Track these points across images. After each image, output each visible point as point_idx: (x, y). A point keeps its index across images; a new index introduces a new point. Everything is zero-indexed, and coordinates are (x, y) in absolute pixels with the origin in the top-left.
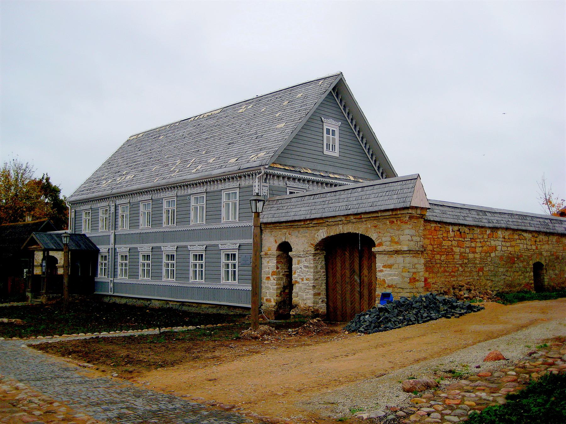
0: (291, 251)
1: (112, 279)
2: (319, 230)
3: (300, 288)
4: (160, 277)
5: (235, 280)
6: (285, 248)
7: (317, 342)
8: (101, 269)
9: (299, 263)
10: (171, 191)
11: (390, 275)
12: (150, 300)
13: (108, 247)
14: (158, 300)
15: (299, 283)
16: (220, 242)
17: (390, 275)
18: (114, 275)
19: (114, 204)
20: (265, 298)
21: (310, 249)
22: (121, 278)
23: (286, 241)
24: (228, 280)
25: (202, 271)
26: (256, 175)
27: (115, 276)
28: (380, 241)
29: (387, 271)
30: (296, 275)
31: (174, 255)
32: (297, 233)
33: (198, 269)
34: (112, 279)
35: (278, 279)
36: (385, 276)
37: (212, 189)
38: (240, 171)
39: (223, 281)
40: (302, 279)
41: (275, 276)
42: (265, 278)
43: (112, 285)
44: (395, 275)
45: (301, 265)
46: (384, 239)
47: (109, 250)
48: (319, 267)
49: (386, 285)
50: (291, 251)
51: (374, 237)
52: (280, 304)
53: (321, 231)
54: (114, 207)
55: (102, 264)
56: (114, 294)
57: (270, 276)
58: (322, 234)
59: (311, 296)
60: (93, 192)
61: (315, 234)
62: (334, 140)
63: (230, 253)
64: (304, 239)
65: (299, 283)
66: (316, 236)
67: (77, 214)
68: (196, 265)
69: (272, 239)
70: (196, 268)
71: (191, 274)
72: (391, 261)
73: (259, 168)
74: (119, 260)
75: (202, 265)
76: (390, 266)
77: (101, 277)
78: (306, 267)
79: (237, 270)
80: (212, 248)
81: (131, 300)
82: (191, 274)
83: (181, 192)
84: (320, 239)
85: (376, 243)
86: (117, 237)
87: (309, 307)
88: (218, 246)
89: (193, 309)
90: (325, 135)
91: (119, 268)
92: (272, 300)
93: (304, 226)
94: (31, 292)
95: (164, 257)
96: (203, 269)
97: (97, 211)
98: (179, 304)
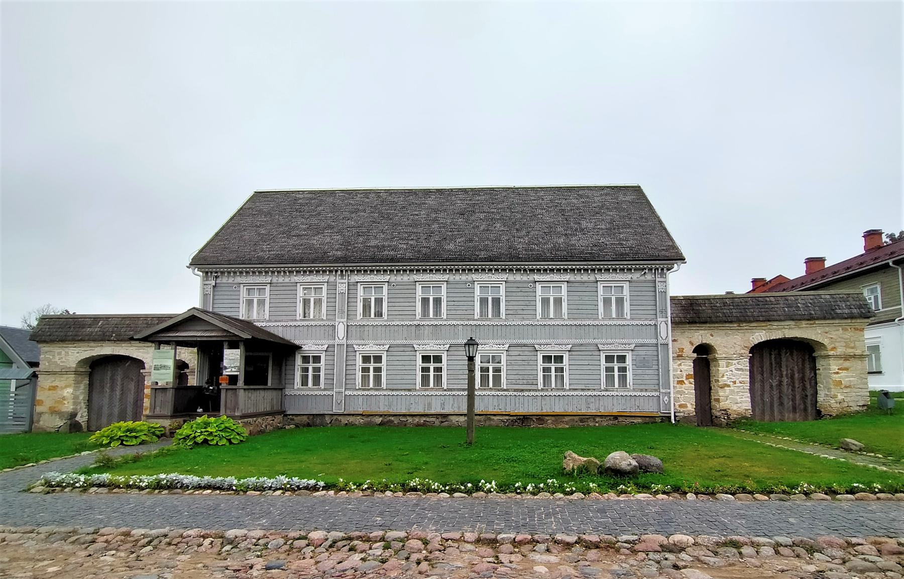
6: (704, 353)
15: (729, 386)
17: (847, 377)
21: (743, 351)
29: (843, 373)
30: (725, 378)
44: (852, 377)
45: (732, 368)
46: (837, 344)
58: (760, 335)
65: (729, 386)
72: (847, 364)
76: (847, 369)
84: (757, 342)
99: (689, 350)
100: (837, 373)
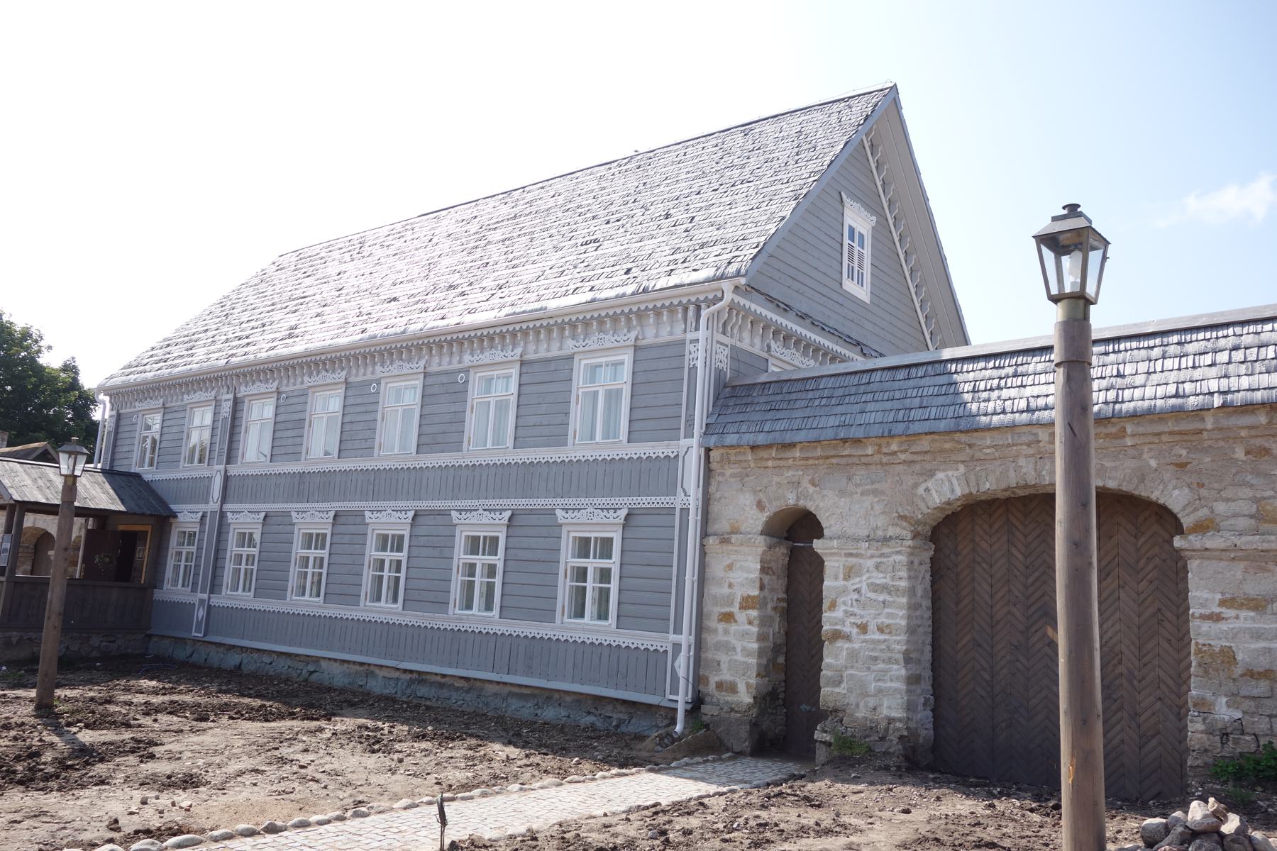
0: (820, 534)
1: (205, 596)
2: (931, 474)
3: (853, 655)
4: (280, 593)
5: (395, 600)
7: (563, 774)
8: (177, 568)
9: (849, 573)
10: (410, 360)
11: (1257, 635)
12: (317, 660)
13: (202, 508)
14: (343, 661)
16: (559, 501)
17: (1257, 635)
18: (213, 586)
19: (231, 396)
20: (713, 680)
22: (235, 596)
23: (802, 503)
24: (379, 599)
25: (397, 579)
26: (698, 308)
27: (214, 588)
28: (1203, 513)
30: (839, 613)
31: (325, 535)
32: (844, 480)
33: (386, 574)
34: (205, 596)
35: (764, 622)
36: (1235, 634)
37: (542, 354)
38: (644, 297)
39: (455, 610)
40: (863, 628)
41: (754, 613)
42: (715, 617)
43: (201, 613)
45: (861, 582)
47: (203, 517)
48: (920, 592)
49: (1238, 671)
50: (820, 534)
51: (1175, 498)
52: (766, 700)
53: (940, 475)
54: (230, 404)
55: (180, 554)
56: (206, 639)
57: (735, 609)
59: (901, 686)
60: (175, 366)
61: (916, 485)
62: (861, 256)
63: (593, 535)
64: (871, 498)
65: (848, 638)
66: (921, 490)
67: (122, 423)
68: (383, 562)
69: (747, 499)
70: (382, 570)
71: (456, 591)
73: (715, 285)
74: (232, 548)
75: (399, 563)
77: (174, 589)
78: (875, 588)
79: (614, 586)
80: (533, 519)
81: (256, 656)
82: (456, 591)
83: (442, 363)
84: (936, 500)
85: (1187, 521)
86: (231, 484)
87: (891, 720)
88: (552, 512)
89: (455, 696)
90: (846, 241)
91: (229, 567)
92: (742, 687)
93: (877, 458)
94: (1185, 807)
95: (371, 542)
96: (402, 575)
97: (181, 415)
98: (408, 676)
99: (755, 520)
100: (1216, 618)
